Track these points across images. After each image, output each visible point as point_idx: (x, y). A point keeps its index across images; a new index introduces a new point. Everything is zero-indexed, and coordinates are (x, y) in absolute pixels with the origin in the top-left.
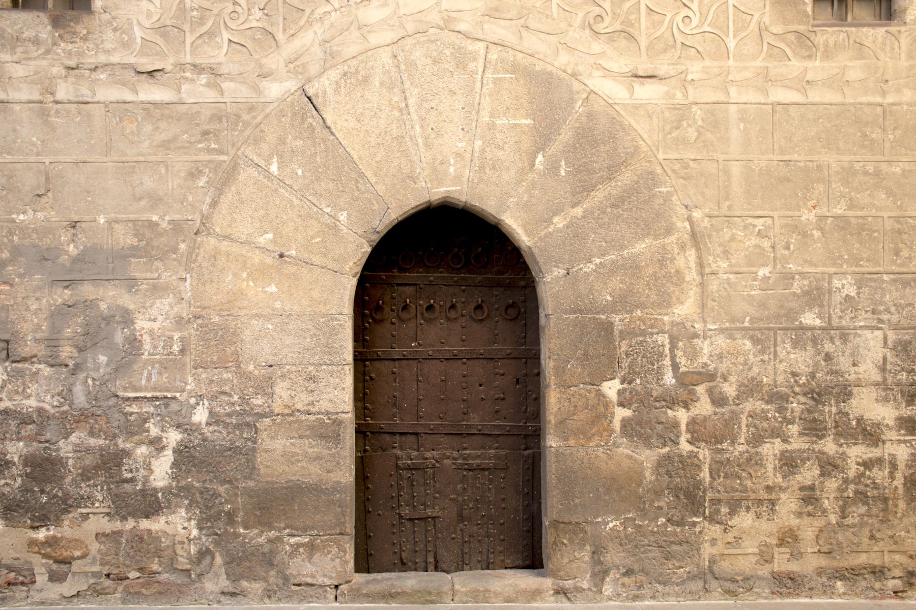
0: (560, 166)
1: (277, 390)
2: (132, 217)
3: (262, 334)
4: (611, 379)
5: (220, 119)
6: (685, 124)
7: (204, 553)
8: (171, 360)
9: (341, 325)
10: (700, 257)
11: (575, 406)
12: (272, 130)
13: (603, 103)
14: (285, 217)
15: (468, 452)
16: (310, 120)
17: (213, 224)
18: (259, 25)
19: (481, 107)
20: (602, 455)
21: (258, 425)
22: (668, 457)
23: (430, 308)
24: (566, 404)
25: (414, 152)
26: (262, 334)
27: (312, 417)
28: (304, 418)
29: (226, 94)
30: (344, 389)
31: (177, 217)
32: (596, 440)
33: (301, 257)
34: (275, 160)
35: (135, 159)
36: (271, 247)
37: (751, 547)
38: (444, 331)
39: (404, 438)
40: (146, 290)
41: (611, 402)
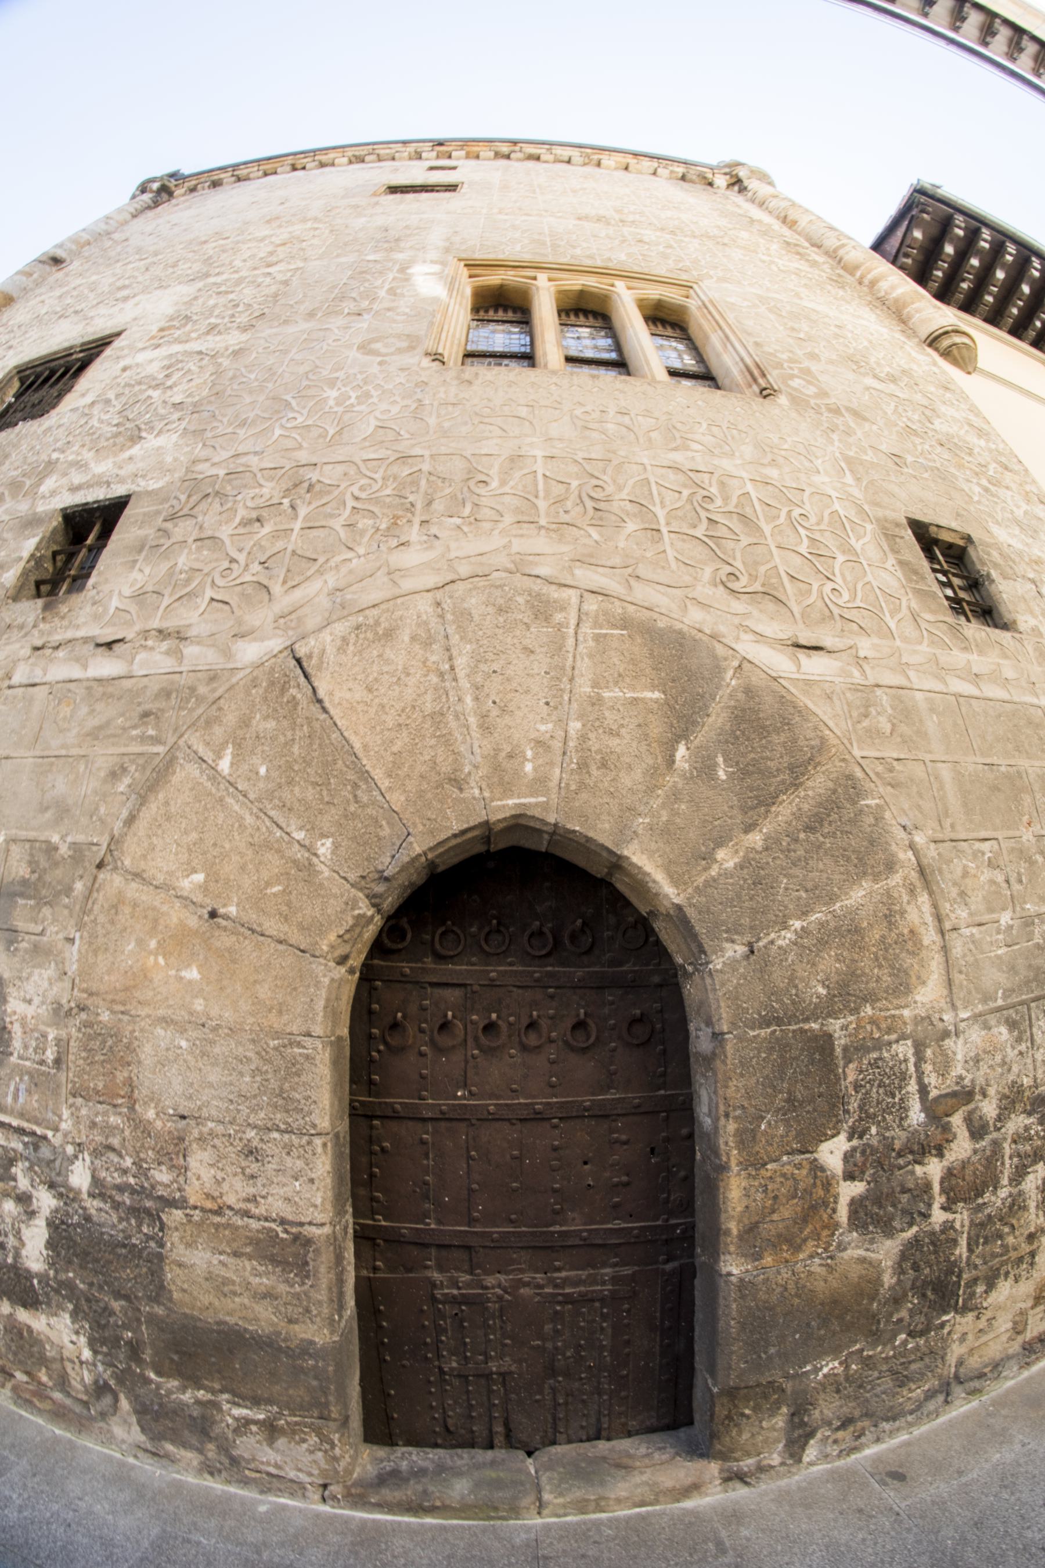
0: (716, 764)
1: (193, 1162)
2: (32, 835)
3: (171, 1055)
4: (833, 1136)
5: (168, 695)
6: (872, 710)
7: (100, 1389)
8: (43, 1074)
9: (307, 1057)
10: (935, 906)
11: (775, 1198)
12: (233, 707)
13: (764, 676)
14: (227, 846)
15: (564, 1274)
16: (293, 691)
17: (122, 853)
18: (255, 579)
19: (576, 672)
20: (818, 1270)
21: (164, 1217)
22: (915, 1243)
23: (490, 1028)
24: (759, 1196)
25: (460, 738)
26: (171, 1055)
27: (254, 1224)
28: (240, 1223)
29: (185, 661)
30: (312, 1181)
31: (81, 838)
32: (810, 1246)
33: (245, 919)
34: (229, 750)
35: (56, 753)
36: (198, 898)
37: (1004, 1324)
38: (514, 1070)
39: (444, 1253)
40: (26, 951)
41: (834, 1176)
